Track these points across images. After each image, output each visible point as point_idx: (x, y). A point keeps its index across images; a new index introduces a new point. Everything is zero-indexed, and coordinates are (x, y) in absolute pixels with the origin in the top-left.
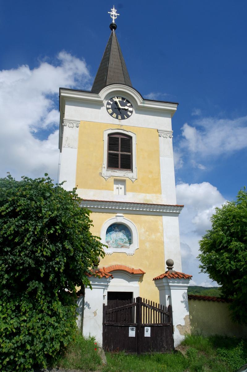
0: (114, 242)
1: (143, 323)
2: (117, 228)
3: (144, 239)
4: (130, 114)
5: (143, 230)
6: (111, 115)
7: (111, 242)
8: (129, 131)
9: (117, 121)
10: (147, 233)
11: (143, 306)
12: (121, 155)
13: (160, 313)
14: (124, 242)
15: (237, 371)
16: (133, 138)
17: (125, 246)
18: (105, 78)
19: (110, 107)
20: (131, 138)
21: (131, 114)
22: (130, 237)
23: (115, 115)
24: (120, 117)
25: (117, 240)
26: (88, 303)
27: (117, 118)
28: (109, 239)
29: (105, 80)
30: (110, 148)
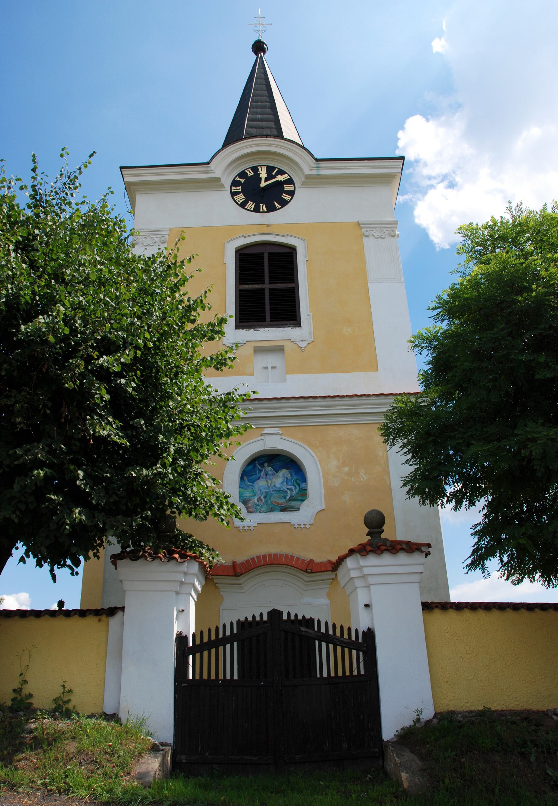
0: (264, 500)
3: (336, 485)
4: (286, 197)
8: (288, 235)
10: (346, 469)
12: (271, 290)
13: (361, 653)
14: (288, 498)
19: (240, 190)
22: (303, 485)
24: (263, 208)
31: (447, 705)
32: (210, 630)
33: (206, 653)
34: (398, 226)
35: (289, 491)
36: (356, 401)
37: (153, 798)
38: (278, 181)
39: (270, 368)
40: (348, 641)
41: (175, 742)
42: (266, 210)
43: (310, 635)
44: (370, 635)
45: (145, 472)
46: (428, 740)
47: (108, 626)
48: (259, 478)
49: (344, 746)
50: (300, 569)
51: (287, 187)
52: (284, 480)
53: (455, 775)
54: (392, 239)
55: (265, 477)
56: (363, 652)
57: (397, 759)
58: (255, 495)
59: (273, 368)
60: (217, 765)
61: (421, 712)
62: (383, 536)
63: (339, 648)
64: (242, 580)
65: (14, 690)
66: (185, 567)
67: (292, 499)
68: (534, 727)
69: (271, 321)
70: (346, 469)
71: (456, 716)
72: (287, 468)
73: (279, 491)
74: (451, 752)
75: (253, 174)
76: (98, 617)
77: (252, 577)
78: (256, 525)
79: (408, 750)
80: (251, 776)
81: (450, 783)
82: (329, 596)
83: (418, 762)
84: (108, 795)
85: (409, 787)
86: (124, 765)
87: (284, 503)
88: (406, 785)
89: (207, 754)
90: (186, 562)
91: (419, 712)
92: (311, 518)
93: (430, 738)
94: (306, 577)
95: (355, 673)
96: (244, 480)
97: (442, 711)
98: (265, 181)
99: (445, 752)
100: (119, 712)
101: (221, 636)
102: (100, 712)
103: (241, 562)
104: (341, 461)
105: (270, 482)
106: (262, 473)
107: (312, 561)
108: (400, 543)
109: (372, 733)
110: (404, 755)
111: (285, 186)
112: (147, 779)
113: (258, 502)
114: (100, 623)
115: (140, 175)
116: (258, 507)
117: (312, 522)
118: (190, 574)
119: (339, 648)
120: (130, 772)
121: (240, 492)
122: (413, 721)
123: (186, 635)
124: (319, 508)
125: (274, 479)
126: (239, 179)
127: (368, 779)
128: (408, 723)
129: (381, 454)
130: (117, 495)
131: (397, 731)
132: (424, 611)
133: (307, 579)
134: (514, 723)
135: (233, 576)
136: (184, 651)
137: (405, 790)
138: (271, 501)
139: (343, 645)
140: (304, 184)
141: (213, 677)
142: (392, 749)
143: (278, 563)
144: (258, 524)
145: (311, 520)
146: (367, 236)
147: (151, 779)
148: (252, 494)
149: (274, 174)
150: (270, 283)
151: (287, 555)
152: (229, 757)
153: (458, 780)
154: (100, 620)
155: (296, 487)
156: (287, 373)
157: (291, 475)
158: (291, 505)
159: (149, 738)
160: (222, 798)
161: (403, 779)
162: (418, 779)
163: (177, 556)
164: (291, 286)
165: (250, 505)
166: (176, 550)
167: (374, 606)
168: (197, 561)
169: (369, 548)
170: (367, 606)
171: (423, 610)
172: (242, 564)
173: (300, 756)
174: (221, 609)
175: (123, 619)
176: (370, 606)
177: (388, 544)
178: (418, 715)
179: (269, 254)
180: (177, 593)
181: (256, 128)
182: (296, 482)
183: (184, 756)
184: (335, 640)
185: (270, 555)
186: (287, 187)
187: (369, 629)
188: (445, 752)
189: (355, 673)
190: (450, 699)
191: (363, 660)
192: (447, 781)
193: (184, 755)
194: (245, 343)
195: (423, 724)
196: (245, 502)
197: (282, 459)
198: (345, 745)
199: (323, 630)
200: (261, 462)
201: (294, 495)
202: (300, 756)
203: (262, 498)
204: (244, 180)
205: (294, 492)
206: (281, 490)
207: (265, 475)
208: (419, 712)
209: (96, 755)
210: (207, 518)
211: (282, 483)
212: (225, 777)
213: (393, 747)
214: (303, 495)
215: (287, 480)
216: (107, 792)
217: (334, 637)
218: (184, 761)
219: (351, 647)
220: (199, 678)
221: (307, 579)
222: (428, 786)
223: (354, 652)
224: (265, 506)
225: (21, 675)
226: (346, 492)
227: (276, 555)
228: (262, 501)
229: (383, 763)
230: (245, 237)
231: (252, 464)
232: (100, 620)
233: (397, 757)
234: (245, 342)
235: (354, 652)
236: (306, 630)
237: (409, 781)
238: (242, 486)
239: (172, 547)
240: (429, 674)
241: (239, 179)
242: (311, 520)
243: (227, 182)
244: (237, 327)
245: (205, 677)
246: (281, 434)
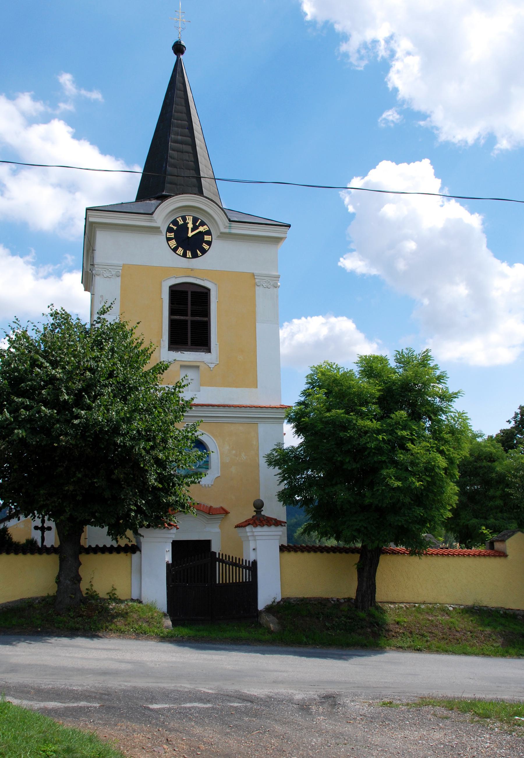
1: (217, 583)
3: (228, 461)
4: (206, 247)
5: (227, 447)
6: (175, 250)
8: (205, 279)
9: (184, 263)
10: (234, 452)
11: (217, 563)
12: (192, 322)
14: (197, 466)
16: (211, 291)
18: (164, 166)
19: (173, 237)
20: (209, 290)
21: (209, 247)
23: (180, 251)
24: (189, 254)
26: (499, 432)
27: (184, 255)
29: (164, 169)
30: (172, 311)
31: (287, 595)
34: (280, 279)
36: (243, 410)
38: (200, 232)
42: (191, 257)
44: (255, 563)
51: (207, 238)
54: (275, 289)
56: (251, 571)
63: (241, 569)
65: (87, 589)
66: (172, 531)
68: (323, 607)
69: (191, 345)
70: (234, 452)
75: (183, 223)
82: (220, 527)
91: (275, 598)
94: (208, 517)
98: (192, 232)
100: (141, 599)
102: (130, 598)
107: (211, 507)
111: (205, 236)
115: (101, 217)
119: (241, 569)
126: (172, 226)
128: (269, 603)
129: (255, 443)
134: (315, 604)
140: (218, 237)
146: (258, 286)
149: (197, 224)
150: (191, 316)
156: (201, 385)
164: (205, 320)
167: (258, 550)
170: (254, 549)
179: (192, 292)
181: (177, 151)
186: (207, 238)
189: (247, 580)
198: (242, 612)
204: (176, 227)
214: (207, 465)
221: (208, 518)
225: (90, 582)
230: (176, 278)
232: (127, 555)
241: (172, 226)
243: (164, 229)
244: (170, 349)
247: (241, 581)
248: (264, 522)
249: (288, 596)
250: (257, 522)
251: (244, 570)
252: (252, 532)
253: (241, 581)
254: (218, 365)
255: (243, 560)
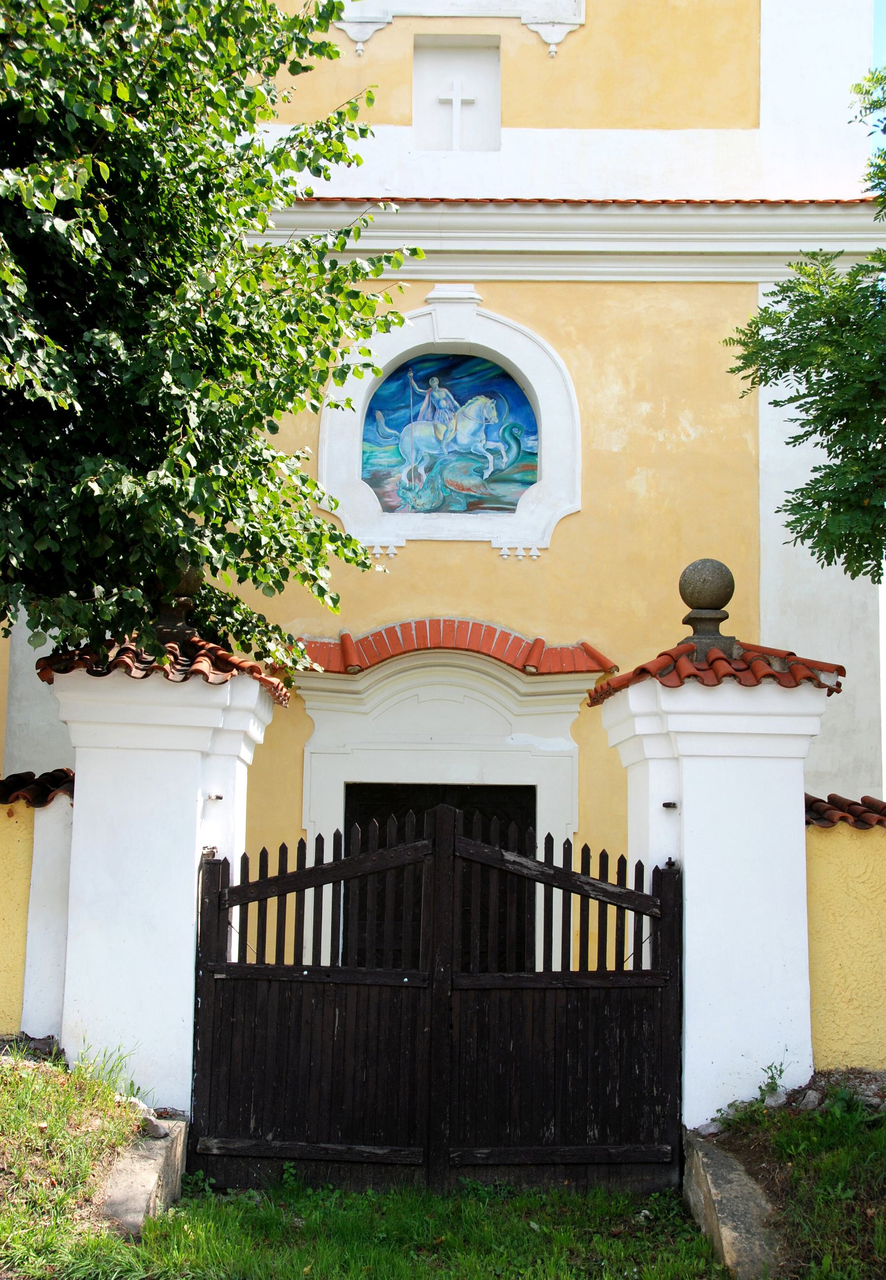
0: (424, 477)
1: (539, 967)
2: (440, 386)
3: (615, 449)
7: (402, 474)
10: (645, 408)
13: (646, 919)
14: (487, 474)
15: (626, 1279)
17: (497, 499)
22: (528, 443)
25: (444, 464)
28: (384, 458)
31: (846, 1054)
32: (283, 850)
33: (272, 903)
35: (490, 457)
37: (146, 1269)
39: (457, 104)
40: (618, 890)
41: (195, 1108)
43: (525, 871)
45: (127, 485)
46: (792, 1150)
47: (33, 827)
48: (415, 418)
49: (591, 1134)
50: (508, 664)
52: (481, 426)
53: (848, 1248)
55: (430, 415)
57: (713, 1191)
58: (403, 462)
59: (467, 103)
60: (292, 1164)
61: (781, 1072)
62: (725, 629)
63: (594, 905)
64: (362, 682)
66: (225, 694)
67: (498, 478)
70: (645, 408)
71: (864, 1086)
72: (490, 395)
73: (466, 454)
74: (844, 1189)
76: (7, 807)
77: (388, 677)
78: (403, 544)
79: (743, 1168)
80: (370, 1192)
81: (836, 1266)
82: (577, 732)
83: (763, 1202)
84: (41, 1261)
85: (738, 1264)
86: (76, 1180)
87: (476, 486)
88: (730, 1258)
89: (270, 1137)
90: (228, 686)
91: (775, 1072)
92: (544, 532)
93: (797, 1146)
94: (522, 683)
95: (629, 966)
96: (375, 420)
97: (832, 1067)
99: (829, 1189)
100: (60, 1034)
101: (310, 863)
103: (361, 636)
104: (633, 386)
105: (442, 428)
106: (425, 404)
107: (538, 643)
108: (767, 654)
109: (658, 1108)
110: (730, 1182)
112: (131, 1218)
113: (410, 480)
114: (13, 819)
116: (410, 495)
117: (546, 543)
118: (237, 709)
120: (90, 1197)
121: (364, 453)
122: (760, 1087)
123: (225, 859)
124: (568, 508)
125: (454, 421)
127: (641, 1218)
130: (54, 535)
131: (719, 1111)
132: (811, 827)
133: (523, 689)
135: (339, 672)
136: (221, 896)
137: (726, 1271)
138: (442, 479)
139: (604, 899)
141: (289, 959)
142: (705, 1160)
143: (454, 646)
144: (408, 541)
145: (543, 538)
147: (139, 1219)
148: (394, 460)
151: (477, 626)
152: (322, 1145)
153: (856, 1262)
154: (10, 814)
155: (509, 445)
156: (503, 123)
157: (500, 414)
158: (493, 492)
159: (133, 1099)
160: (306, 1269)
161: (724, 1242)
162: (761, 1245)
163: (204, 665)
165: (388, 488)
166: (202, 647)
167: (687, 808)
168: (255, 678)
169: (686, 666)
170: (668, 806)
171: (808, 823)
172: (363, 641)
173: (486, 1151)
174: (307, 755)
175: (70, 814)
176: (678, 805)
177: (736, 652)
178: (772, 1078)
180: (205, 755)
182: (512, 434)
183: (215, 1141)
184: (587, 888)
185: (435, 623)
187: (670, 863)
188: (829, 1189)
189: (629, 966)
190: (854, 1042)
191: (651, 935)
192: (827, 1261)
193: (215, 1138)
194: (389, 23)
195: (783, 1099)
196: (375, 480)
197: (478, 368)
198: (594, 1133)
199: (558, 861)
200: (421, 373)
201: (503, 467)
202: (486, 1151)
203: (421, 470)
205: (505, 460)
206: (471, 453)
207: (430, 410)
208: (774, 1071)
209: (9, 1156)
210: (283, 586)
211: (474, 434)
212: (310, 1191)
213: (706, 1155)
215: (487, 427)
216: (38, 1253)
217: (583, 878)
218: (215, 1151)
219: (624, 905)
220: (254, 962)
221: (523, 689)
222: (782, 1267)
223: (630, 915)
224: (428, 492)
226: (638, 469)
227: (449, 623)
228: (420, 480)
229: (682, 1174)
231: (398, 379)
232: (10, 814)
233: (717, 1186)
234: (390, 19)
235: (630, 915)
236: (518, 859)
237: (739, 1250)
238: (371, 436)
239: (193, 634)
240: (808, 982)
242: (543, 538)
245: (270, 958)
246: (479, 303)
247: (593, 966)
248: (723, 667)
249: (856, 1064)
250: (686, 666)
251: (612, 910)
252: (661, 715)
253: (593, 966)
254: (583, 32)
255: (622, 862)
